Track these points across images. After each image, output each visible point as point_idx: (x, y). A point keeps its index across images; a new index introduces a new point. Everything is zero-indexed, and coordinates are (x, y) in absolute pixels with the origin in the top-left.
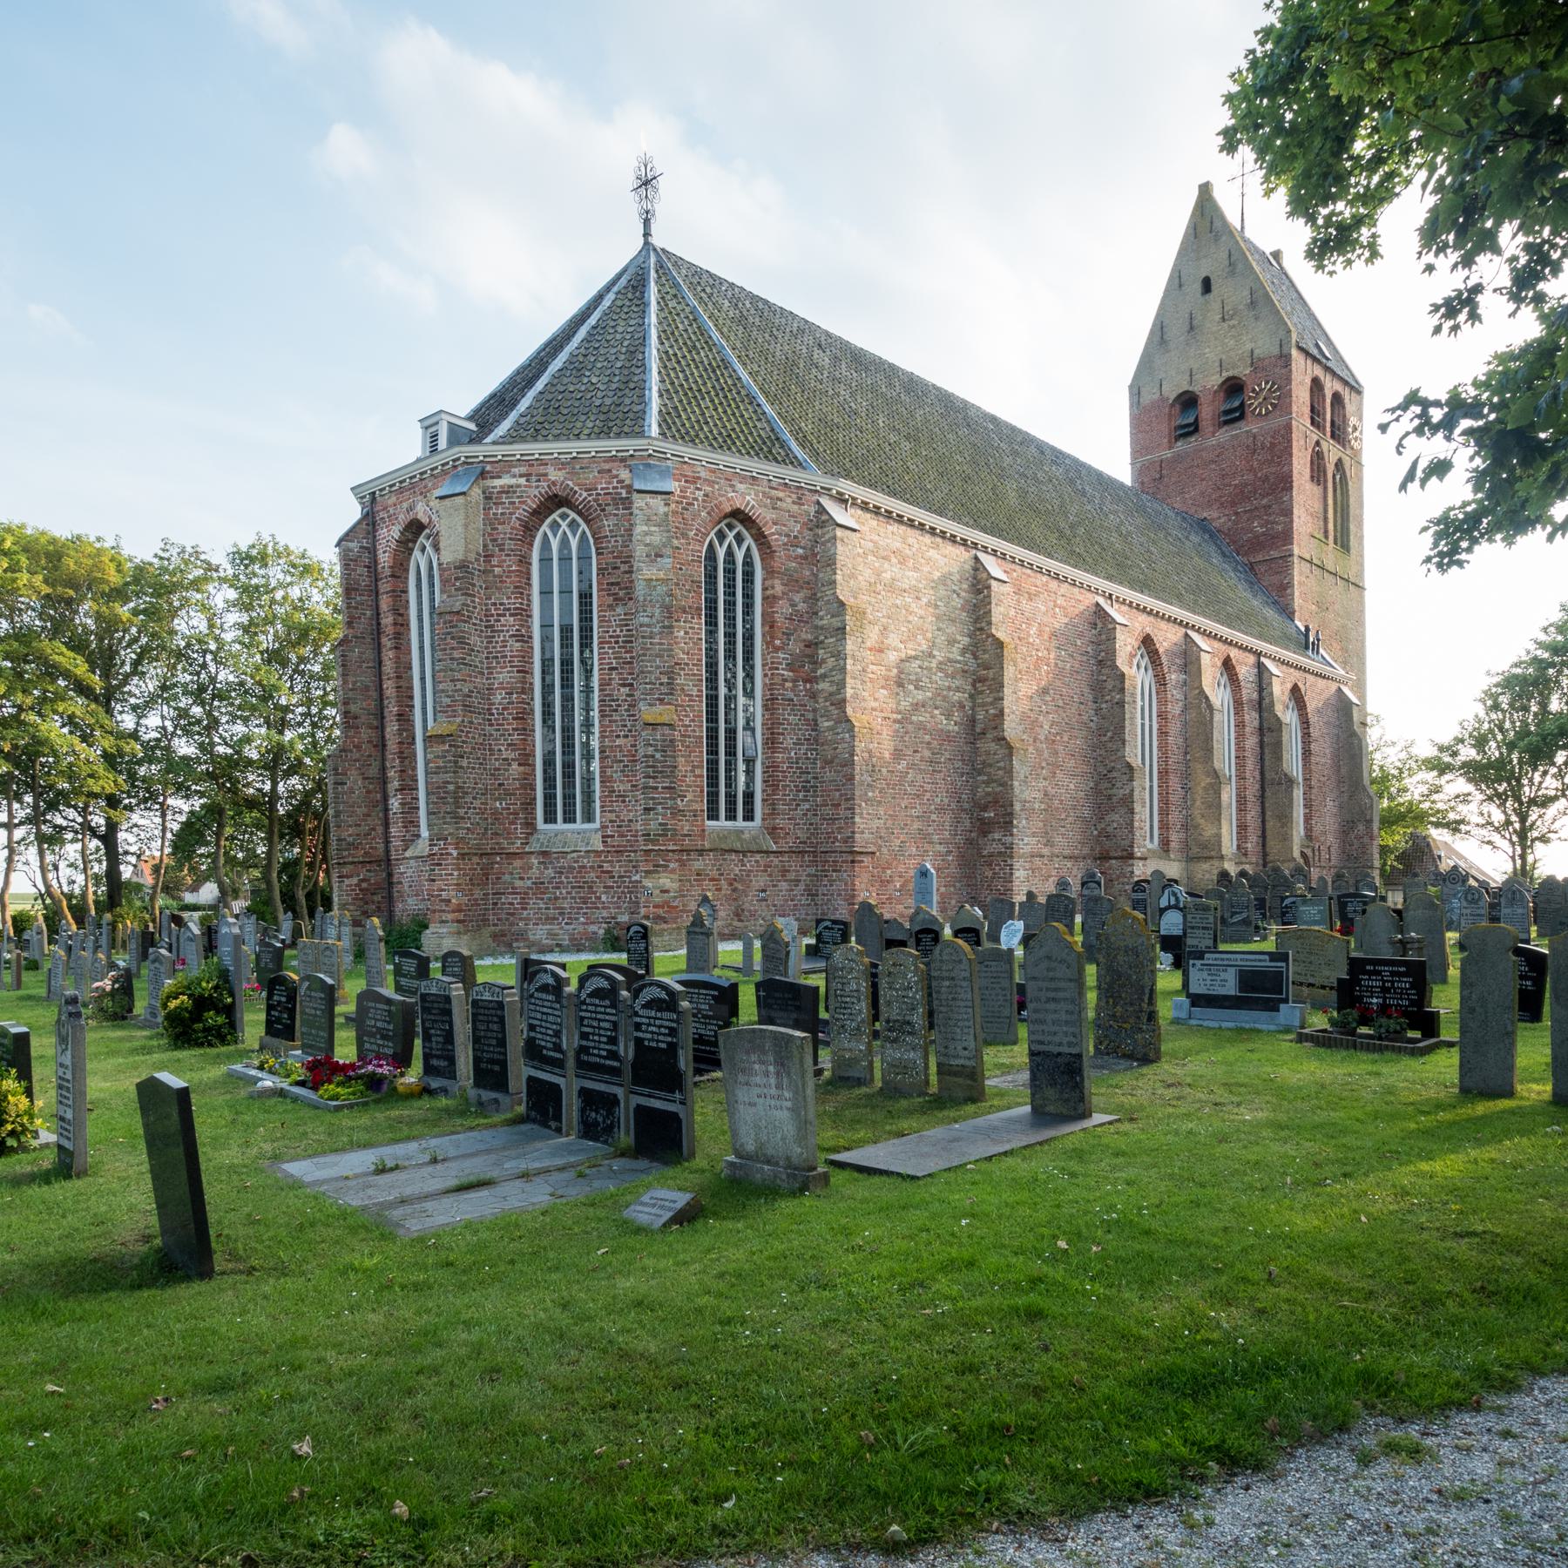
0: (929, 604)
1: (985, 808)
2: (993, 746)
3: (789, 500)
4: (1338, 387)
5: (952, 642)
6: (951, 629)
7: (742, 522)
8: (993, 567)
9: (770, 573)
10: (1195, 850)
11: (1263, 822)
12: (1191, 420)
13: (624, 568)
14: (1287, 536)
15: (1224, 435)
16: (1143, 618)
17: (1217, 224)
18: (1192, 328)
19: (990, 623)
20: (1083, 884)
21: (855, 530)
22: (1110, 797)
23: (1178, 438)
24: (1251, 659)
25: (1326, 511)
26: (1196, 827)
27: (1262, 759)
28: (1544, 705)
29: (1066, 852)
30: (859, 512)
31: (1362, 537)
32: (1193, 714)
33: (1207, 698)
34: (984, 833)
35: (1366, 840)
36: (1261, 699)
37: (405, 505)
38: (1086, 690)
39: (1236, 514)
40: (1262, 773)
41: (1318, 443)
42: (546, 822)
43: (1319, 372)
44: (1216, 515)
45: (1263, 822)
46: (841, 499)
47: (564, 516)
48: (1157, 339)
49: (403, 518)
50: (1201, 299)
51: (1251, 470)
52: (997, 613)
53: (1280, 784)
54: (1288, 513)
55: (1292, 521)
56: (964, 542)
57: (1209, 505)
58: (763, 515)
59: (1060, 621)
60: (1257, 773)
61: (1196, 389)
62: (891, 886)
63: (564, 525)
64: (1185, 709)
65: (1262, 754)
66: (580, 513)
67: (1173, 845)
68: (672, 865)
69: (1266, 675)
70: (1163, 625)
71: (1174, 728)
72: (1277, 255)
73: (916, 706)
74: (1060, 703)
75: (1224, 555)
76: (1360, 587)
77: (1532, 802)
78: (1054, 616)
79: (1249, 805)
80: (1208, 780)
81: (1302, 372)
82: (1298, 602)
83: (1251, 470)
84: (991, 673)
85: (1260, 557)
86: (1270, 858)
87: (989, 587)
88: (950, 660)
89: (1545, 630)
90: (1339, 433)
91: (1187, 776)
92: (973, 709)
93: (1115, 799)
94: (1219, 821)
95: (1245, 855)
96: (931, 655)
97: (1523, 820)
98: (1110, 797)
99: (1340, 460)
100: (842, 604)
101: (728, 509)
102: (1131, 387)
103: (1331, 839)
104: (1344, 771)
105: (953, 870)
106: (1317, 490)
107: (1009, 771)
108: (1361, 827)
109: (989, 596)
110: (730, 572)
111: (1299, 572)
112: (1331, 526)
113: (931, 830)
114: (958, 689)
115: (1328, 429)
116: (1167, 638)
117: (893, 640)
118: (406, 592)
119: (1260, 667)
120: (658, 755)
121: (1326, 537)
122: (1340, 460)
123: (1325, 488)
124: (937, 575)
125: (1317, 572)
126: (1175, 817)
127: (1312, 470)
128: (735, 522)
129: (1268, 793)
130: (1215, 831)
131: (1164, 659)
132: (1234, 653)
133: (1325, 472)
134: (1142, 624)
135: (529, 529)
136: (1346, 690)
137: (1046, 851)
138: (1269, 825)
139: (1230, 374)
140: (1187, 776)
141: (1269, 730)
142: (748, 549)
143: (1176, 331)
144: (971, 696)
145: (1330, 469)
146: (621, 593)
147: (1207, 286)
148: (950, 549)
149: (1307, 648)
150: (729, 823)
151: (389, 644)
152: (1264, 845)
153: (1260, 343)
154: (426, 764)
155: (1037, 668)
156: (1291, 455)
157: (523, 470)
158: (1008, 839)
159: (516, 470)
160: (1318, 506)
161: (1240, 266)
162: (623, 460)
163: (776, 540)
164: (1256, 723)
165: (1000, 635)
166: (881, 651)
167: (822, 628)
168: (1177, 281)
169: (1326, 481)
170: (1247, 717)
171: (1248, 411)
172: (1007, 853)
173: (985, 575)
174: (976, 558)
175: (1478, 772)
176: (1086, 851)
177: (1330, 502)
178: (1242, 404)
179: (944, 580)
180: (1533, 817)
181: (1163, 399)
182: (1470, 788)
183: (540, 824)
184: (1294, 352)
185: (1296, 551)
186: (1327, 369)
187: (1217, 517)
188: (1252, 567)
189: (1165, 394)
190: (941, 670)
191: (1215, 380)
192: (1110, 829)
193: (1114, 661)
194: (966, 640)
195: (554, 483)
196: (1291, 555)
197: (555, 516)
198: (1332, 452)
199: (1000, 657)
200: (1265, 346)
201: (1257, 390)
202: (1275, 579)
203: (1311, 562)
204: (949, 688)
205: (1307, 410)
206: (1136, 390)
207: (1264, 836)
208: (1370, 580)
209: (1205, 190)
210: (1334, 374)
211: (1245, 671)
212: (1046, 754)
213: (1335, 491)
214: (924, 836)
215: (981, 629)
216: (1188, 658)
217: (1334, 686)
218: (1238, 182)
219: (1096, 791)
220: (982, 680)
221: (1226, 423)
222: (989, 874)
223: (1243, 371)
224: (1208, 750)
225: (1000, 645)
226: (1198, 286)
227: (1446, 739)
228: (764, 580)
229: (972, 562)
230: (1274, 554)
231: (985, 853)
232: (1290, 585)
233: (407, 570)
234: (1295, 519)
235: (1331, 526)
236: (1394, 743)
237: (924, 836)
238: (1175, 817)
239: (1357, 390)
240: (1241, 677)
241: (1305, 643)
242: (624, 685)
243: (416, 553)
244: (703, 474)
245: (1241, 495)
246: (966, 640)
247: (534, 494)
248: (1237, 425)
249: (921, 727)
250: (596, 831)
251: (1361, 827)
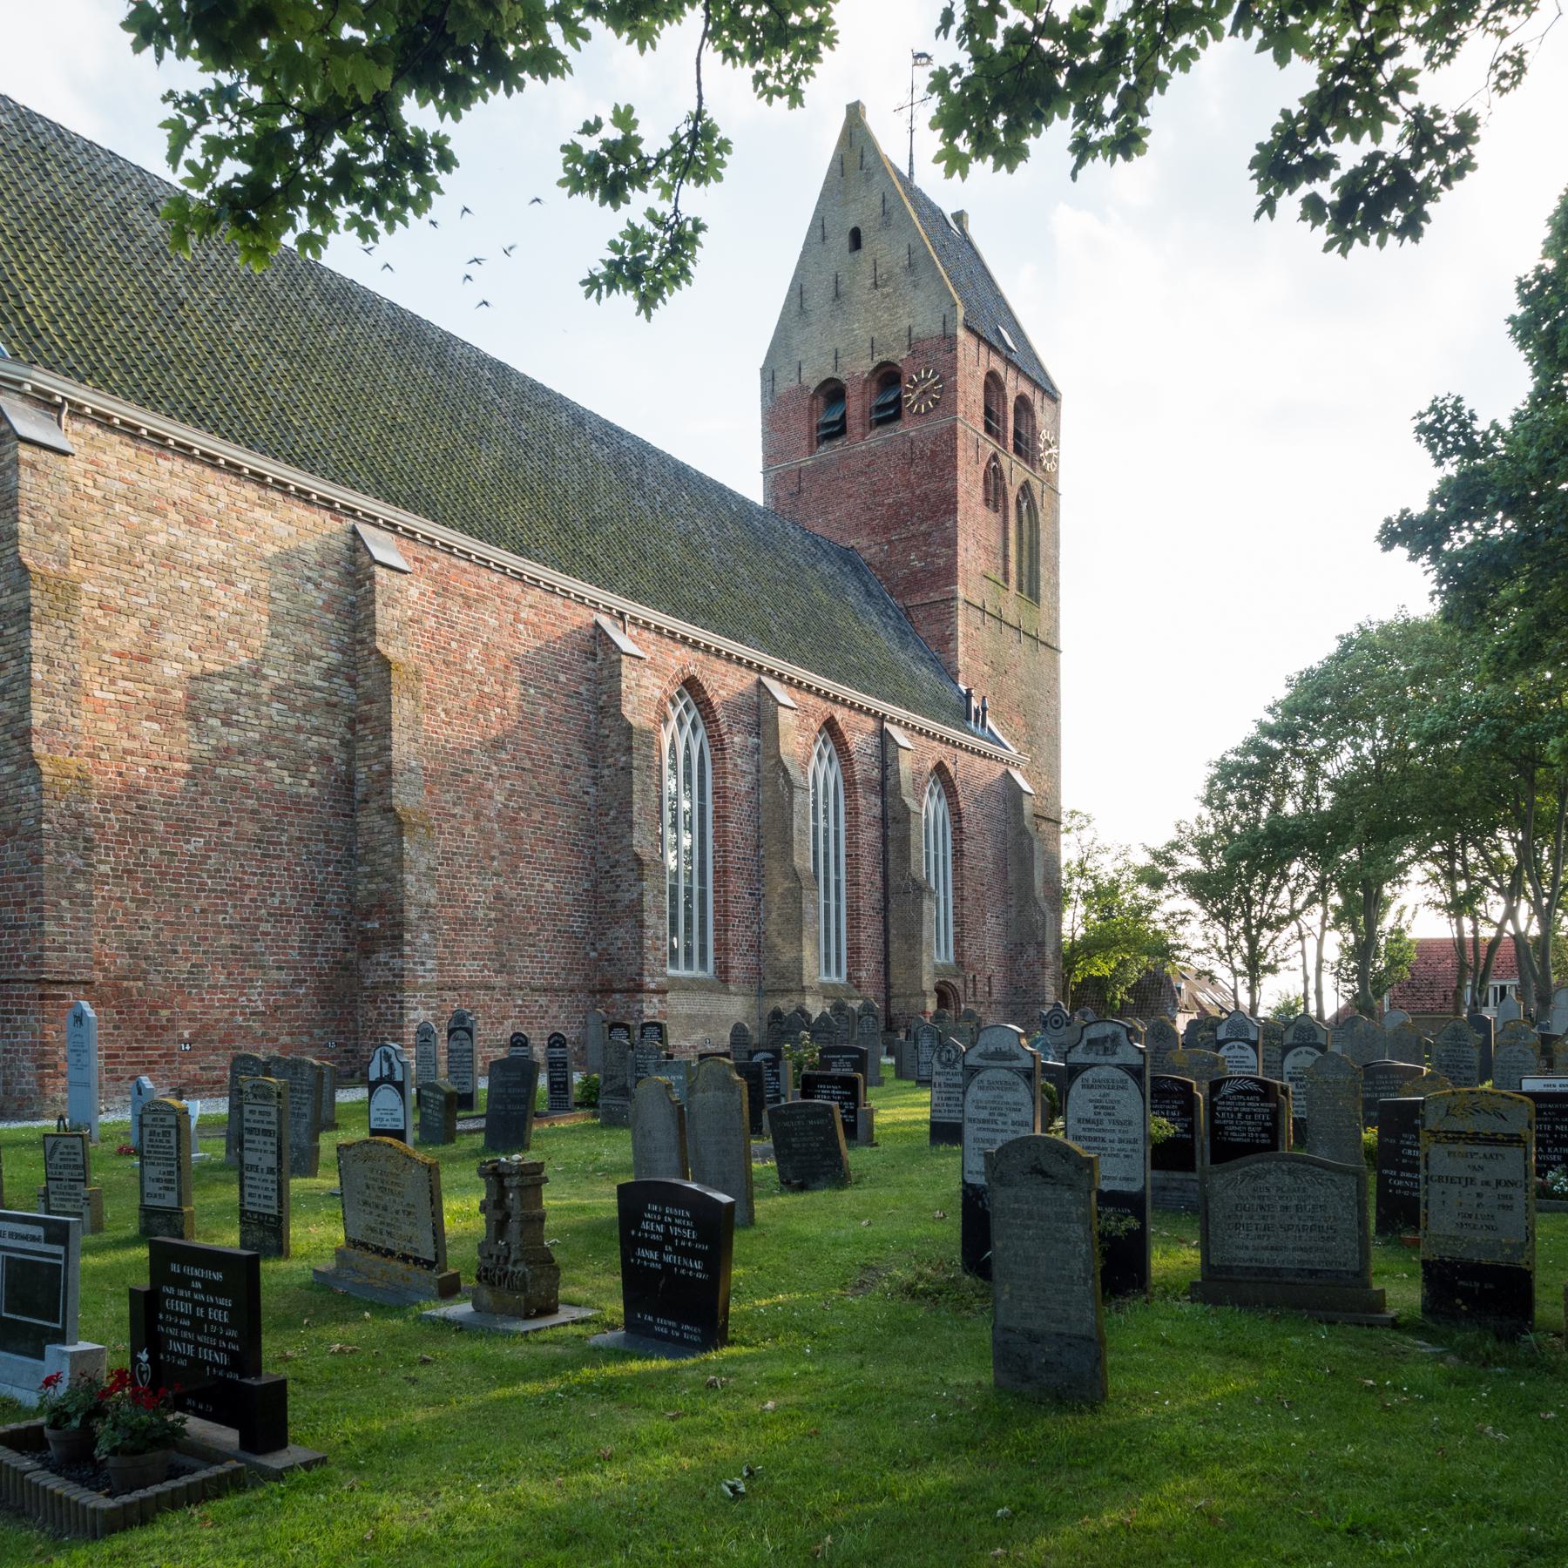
0: (253, 594)
1: (367, 916)
2: (377, 821)
4: (1026, 388)
5: (302, 657)
6: (302, 638)
8: (382, 547)
10: (769, 981)
11: (886, 943)
12: (837, 417)
14: (948, 574)
15: (877, 439)
16: (683, 652)
17: (869, 158)
18: (837, 295)
19: (373, 632)
20: (451, 1032)
21: (65, 454)
22: (613, 904)
23: (819, 443)
24: (870, 724)
25: (1006, 546)
26: (772, 948)
27: (885, 860)
28: (1276, 807)
29: (537, 983)
30: (93, 430)
31: (1057, 585)
32: (766, 794)
33: (785, 770)
34: (367, 953)
35: (1037, 968)
36: (884, 778)
38: (576, 748)
39: (890, 542)
40: (885, 878)
41: (995, 457)
43: (997, 364)
44: (864, 542)
45: (886, 943)
46: (45, 402)
48: (795, 307)
51: (908, 485)
52: (385, 618)
53: (906, 892)
54: (951, 543)
55: (956, 554)
56: (328, 505)
57: (857, 529)
59: (526, 643)
60: (877, 879)
61: (842, 376)
62: (169, 1036)
64: (757, 786)
65: (885, 852)
67: (734, 973)
69: (891, 747)
70: (720, 666)
71: (738, 813)
72: (959, 217)
73: (225, 753)
74: (528, 764)
75: (869, 594)
76: (1058, 650)
77: (1264, 923)
78: (515, 634)
79: (864, 921)
80: (787, 884)
81: (972, 363)
82: (962, 660)
83: (908, 485)
84: (374, 710)
85: (918, 600)
86: (894, 991)
87: (372, 577)
88: (300, 686)
89: (1271, 710)
90: (1026, 447)
91: (757, 879)
92: (349, 763)
93: (619, 907)
94: (800, 939)
95: (858, 987)
96: (257, 674)
97: (1253, 942)
98: (613, 904)
99: (1027, 482)
100: (25, 569)
102: (763, 370)
103: (992, 967)
104: (1011, 878)
105: (306, 1008)
106: (995, 519)
107: (399, 859)
108: (1032, 951)
109: (372, 591)
111: (965, 623)
112: (1013, 566)
113: (257, 947)
114: (316, 731)
115: (1010, 441)
116: (726, 684)
117: (172, 642)
119: (884, 737)
121: (1006, 580)
122: (1027, 482)
123: (1006, 517)
124: (270, 550)
125: (993, 623)
126: (738, 934)
127: (986, 491)
129: (893, 905)
130: (794, 954)
131: (721, 714)
132: (840, 714)
133: (1005, 500)
134: (680, 660)
136: (1017, 776)
137: (499, 981)
138: (894, 947)
139: (884, 357)
140: (757, 879)
141: (894, 822)
143: (819, 298)
144: (345, 744)
145: (1013, 493)
147: (856, 239)
148: (298, 511)
149: (968, 718)
152: (887, 974)
153: (919, 318)
155: (480, 708)
156: (955, 468)
158: (397, 962)
160: (995, 539)
161: (896, 215)
164: (877, 811)
165: (391, 652)
166: (147, 660)
168: (819, 230)
169: (1006, 508)
170: (862, 801)
172: (396, 984)
173: (366, 559)
174: (355, 532)
175: (1200, 886)
176: (575, 980)
177: (1012, 534)
178: (898, 400)
179: (286, 560)
180: (1263, 943)
181: (803, 388)
182: (1193, 905)
184: (961, 333)
185: (961, 593)
186: (1009, 362)
187: (864, 545)
188: (908, 611)
189: (805, 381)
190: (280, 699)
191: (865, 366)
192: (613, 950)
193: (618, 707)
194: (334, 657)
196: (955, 598)
198: (1016, 472)
199: (387, 683)
200: (926, 324)
201: (918, 379)
202: (935, 629)
203: (983, 610)
204: (299, 729)
205: (980, 412)
206: (769, 375)
207: (886, 962)
208: (1067, 639)
209: (855, 112)
210: (1019, 370)
211: (859, 736)
212: (499, 838)
213: (1020, 521)
214: (242, 956)
215: (362, 642)
216: (759, 714)
217: (999, 769)
218: (906, 112)
219: (594, 894)
220: (364, 719)
221: (881, 422)
222: (373, 1015)
223: (899, 355)
224: (787, 842)
225: (386, 664)
226: (845, 240)
227: (1159, 845)
229: (348, 538)
230: (935, 596)
231: (368, 983)
232: (953, 637)
234: (960, 551)
235: (1013, 566)
236: (1107, 850)
237: (242, 956)
238: (738, 934)
239: (1051, 395)
240: (852, 748)
241: (963, 712)
245: (895, 519)
246: (334, 657)
248: (891, 426)
249: (233, 785)
251: (1032, 951)
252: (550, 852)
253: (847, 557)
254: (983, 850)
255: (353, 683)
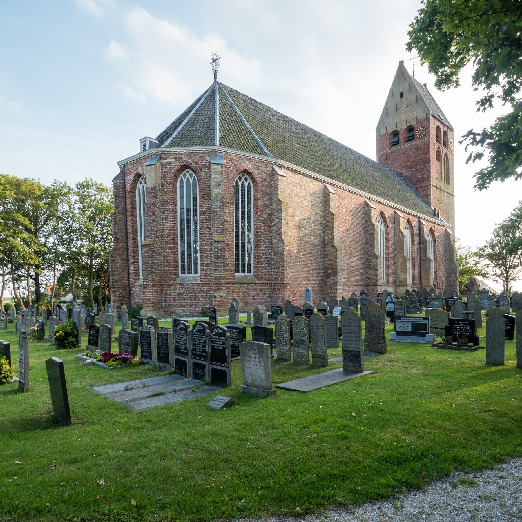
0: (309, 201)
1: (328, 269)
2: (331, 248)
3: (263, 167)
4: (445, 129)
5: (317, 214)
6: (317, 210)
7: (247, 174)
8: (331, 189)
9: (256, 191)
10: (398, 283)
11: (421, 274)
12: (397, 140)
13: (208, 189)
14: (428, 179)
15: (408, 145)
16: (380, 206)
17: (405, 74)
18: (397, 109)
19: (329, 207)
21: (284, 177)
22: (369, 265)
23: (392, 146)
24: (417, 219)
25: (441, 170)
26: (398, 275)
27: (420, 253)
28: (514, 235)
29: (355, 284)
30: (286, 170)
31: (453, 179)
32: (397, 238)
33: (402, 232)
34: (328, 277)
35: (455, 280)
36: (420, 233)
37: (135, 168)
38: (362, 230)
39: (412, 171)
40: (420, 257)
41: (439, 148)
42: (182, 274)
43: (439, 124)
44: (405, 171)
45: (421, 274)
46: (280, 166)
47: (188, 172)
48: (385, 113)
49: (134, 173)
50: (400, 100)
51: (417, 156)
52: (332, 204)
53: (426, 261)
54: (429, 171)
55: (430, 174)
56: (321, 181)
57: (403, 168)
58: (254, 171)
59: (353, 207)
60: (418, 257)
61: (398, 129)
62: (297, 295)
63: (188, 175)
64: (395, 236)
65: (420, 251)
66: (193, 171)
67: (390, 281)
68: (224, 288)
69: (421, 225)
70: (387, 208)
71: (391, 242)
72: (425, 85)
73: (305, 235)
74: (353, 234)
75: (407, 185)
76: (453, 196)
77: (510, 267)
78: (351, 205)
79: (416, 268)
80: (402, 260)
81: (433, 124)
82: (432, 200)
83: (417, 156)
84: (330, 224)
85: (419, 186)
86: (423, 286)
87: (329, 195)
88: (316, 220)
89: (514, 210)
90: (446, 144)
91: (395, 258)
92: (324, 236)
93: (371, 266)
94: (406, 273)
95: (415, 285)
96: (310, 218)
97: (507, 273)
98: (369, 265)
99: (446, 153)
100: (280, 201)
101: (242, 170)
102: (376, 129)
103: (443, 279)
104: (447, 257)
105: (317, 290)
106: (439, 163)
107: (336, 257)
108: (453, 275)
109: (329, 198)
110: (243, 191)
111: (432, 191)
112: (443, 175)
113: (310, 276)
114: (319, 229)
115: (442, 143)
116: (389, 212)
117: (297, 213)
118: (135, 197)
119: (420, 222)
120: (219, 252)
121: (442, 179)
122: (446, 153)
123: (441, 163)
124: (312, 191)
125: (438, 190)
126: (391, 272)
127: (437, 156)
128: (245, 174)
129: (422, 264)
130: (404, 277)
131: (388, 219)
132: (411, 217)
134: (380, 208)
135: (176, 176)
136: (448, 230)
137: (348, 283)
138: (423, 275)
139: (410, 124)
140: (395, 258)
141: (422, 243)
142: (249, 183)
143: (392, 110)
144: (323, 232)
145: (443, 156)
146: (207, 198)
147: (402, 95)
148: (316, 183)
149: (435, 216)
150: (243, 274)
151: (129, 214)
152: (421, 281)
153: (419, 114)
154: (142, 254)
155: (345, 222)
156: (430, 151)
157: (174, 156)
158: (336, 279)
159: (172, 157)
160: (439, 169)
161: (413, 89)
162: (207, 153)
163: (258, 180)
164: (418, 241)
165: (333, 211)
166: (293, 217)
167: (274, 209)
168: (392, 93)
169: (441, 160)
170: (415, 239)
171: (415, 137)
172: (335, 284)
173: (328, 192)
174: (325, 186)
175: (492, 257)
176: (361, 283)
177: (443, 167)
178: (414, 135)
179: (314, 193)
180: (510, 272)
181: (387, 133)
182: (489, 262)
183: (180, 274)
184: (431, 117)
185: (431, 184)
186: (442, 123)
188: (417, 189)
189: (388, 131)
190: (313, 223)
191: (405, 127)
192: (369, 276)
193: (371, 220)
194: (322, 213)
195: (184, 161)
196: (430, 185)
197: (185, 172)
198: (443, 151)
199: (333, 219)
200: (421, 115)
201: (418, 130)
202: (425, 193)
203: (436, 187)
204: (316, 229)
205: (435, 137)
206: (378, 130)
207: (421, 278)
208: (456, 193)
209: (401, 63)
210: (444, 124)
211: (415, 223)
212: (348, 251)
213: (444, 163)
215: (327, 209)
216: (396, 219)
217: (444, 228)
218: (412, 60)
219: (365, 263)
220: (327, 226)
221: (408, 141)
222: (329, 291)
223: (414, 124)
224: (402, 250)
225: (333, 215)
226: (399, 95)
227: (481, 246)
228: (254, 193)
229: (324, 187)
230: (424, 184)
231: (328, 284)
232: (429, 195)
233: (135, 190)
234: (431, 173)
235: (443, 175)
236: (464, 248)
237: (308, 278)
238: (391, 272)
239: (452, 130)
240: (413, 225)
241: (435, 214)
242: (208, 228)
243: (139, 184)
244: (234, 158)
245: (413, 165)
246: (322, 213)
247: (178, 165)
248: (412, 141)
249: (307, 242)
250: (199, 277)
251: (453, 275)
252: (357, 254)
253: (400, 175)
254: (440, 249)
255: (325, 219)
